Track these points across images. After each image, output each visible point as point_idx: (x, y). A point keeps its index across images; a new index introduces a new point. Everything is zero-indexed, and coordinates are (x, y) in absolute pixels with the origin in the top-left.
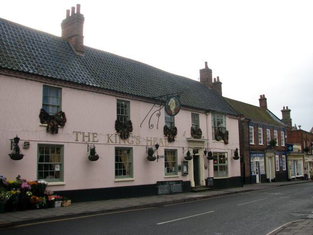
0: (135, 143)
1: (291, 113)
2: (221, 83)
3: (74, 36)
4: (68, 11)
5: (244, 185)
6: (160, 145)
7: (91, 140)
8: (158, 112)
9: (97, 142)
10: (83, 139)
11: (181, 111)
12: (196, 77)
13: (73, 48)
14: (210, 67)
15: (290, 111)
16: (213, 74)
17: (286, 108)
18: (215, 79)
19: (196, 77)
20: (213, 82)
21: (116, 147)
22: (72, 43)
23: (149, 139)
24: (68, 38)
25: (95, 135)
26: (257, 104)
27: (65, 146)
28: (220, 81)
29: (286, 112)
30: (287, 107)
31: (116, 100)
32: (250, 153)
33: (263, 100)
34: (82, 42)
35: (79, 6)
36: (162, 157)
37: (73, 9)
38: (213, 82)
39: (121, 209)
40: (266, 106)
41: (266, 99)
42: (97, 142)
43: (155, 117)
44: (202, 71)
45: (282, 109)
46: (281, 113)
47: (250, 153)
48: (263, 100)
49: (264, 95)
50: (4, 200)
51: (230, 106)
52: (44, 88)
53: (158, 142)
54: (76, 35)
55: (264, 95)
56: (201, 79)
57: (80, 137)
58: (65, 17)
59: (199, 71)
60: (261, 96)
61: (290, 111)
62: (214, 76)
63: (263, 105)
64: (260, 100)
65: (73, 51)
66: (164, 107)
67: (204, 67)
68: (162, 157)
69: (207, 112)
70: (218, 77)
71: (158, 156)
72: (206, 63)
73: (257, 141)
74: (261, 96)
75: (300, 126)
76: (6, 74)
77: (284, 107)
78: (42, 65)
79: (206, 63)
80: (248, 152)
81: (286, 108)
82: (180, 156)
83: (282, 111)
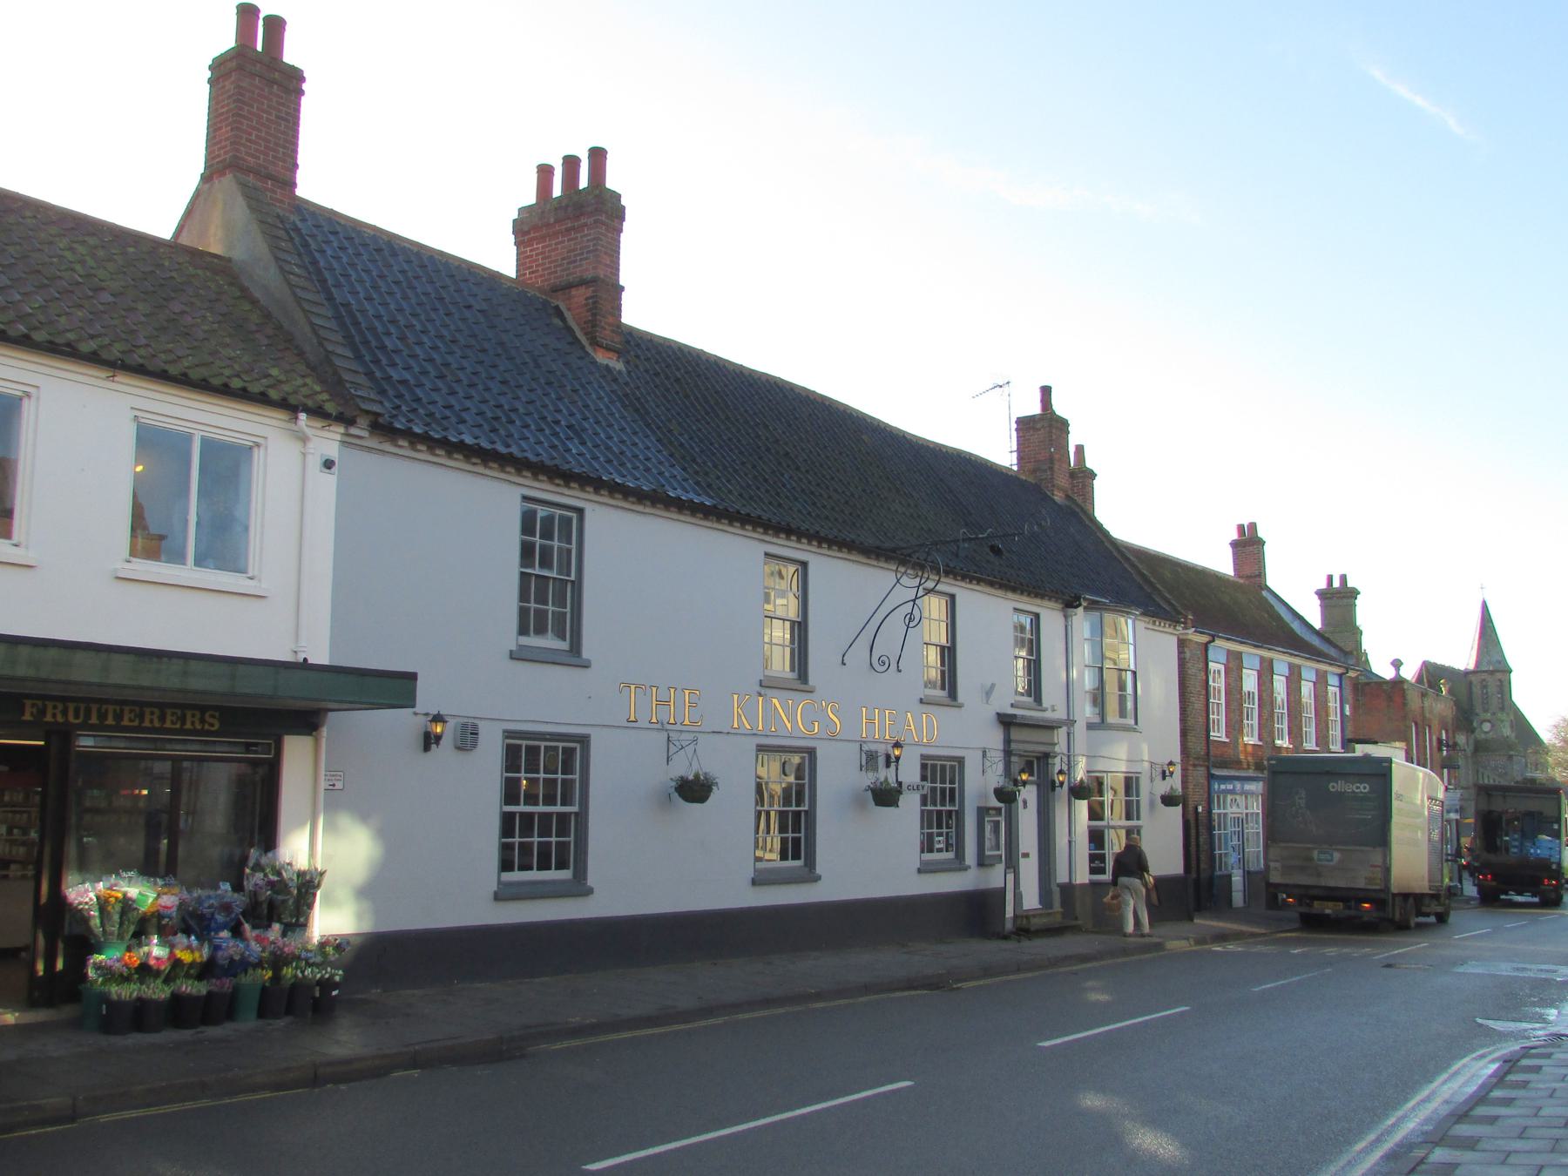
1: (1361, 604)
2: (1092, 475)
3: (583, 283)
4: (545, 172)
12: (1001, 451)
13: (579, 334)
14: (1060, 408)
15: (1354, 593)
17: (1336, 584)
21: (923, 757)
22: (573, 308)
24: (555, 290)
26: (1223, 563)
27: (593, 739)
28: (1089, 464)
29: (1339, 598)
30: (1343, 578)
31: (519, 499)
32: (1211, 777)
33: (1248, 545)
35: (598, 155)
36: (911, 788)
37: (571, 163)
40: (1260, 574)
41: (1261, 543)
44: (1025, 426)
45: (1323, 585)
46: (1316, 602)
47: (1211, 777)
48: (1248, 545)
49: (1253, 526)
50: (1536, 766)
54: (594, 281)
55: (1253, 526)
56: (1020, 459)
59: (1095, 471)
60: (1241, 528)
61: (1354, 593)
63: (1247, 571)
64: (1234, 544)
65: (583, 348)
67: (1035, 409)
71: (900, 784)
72: (1046, 392)
73: (1235, 727)
74: (1241, 528)
75: (1397, 664)
76: (1334, 717)
77: (1330, 578)
78: (508, 416)
79: (1046, 392)
80: (1202, 771)
81: (1336, 584)
82: (981, 781)
83: (1321, 594)
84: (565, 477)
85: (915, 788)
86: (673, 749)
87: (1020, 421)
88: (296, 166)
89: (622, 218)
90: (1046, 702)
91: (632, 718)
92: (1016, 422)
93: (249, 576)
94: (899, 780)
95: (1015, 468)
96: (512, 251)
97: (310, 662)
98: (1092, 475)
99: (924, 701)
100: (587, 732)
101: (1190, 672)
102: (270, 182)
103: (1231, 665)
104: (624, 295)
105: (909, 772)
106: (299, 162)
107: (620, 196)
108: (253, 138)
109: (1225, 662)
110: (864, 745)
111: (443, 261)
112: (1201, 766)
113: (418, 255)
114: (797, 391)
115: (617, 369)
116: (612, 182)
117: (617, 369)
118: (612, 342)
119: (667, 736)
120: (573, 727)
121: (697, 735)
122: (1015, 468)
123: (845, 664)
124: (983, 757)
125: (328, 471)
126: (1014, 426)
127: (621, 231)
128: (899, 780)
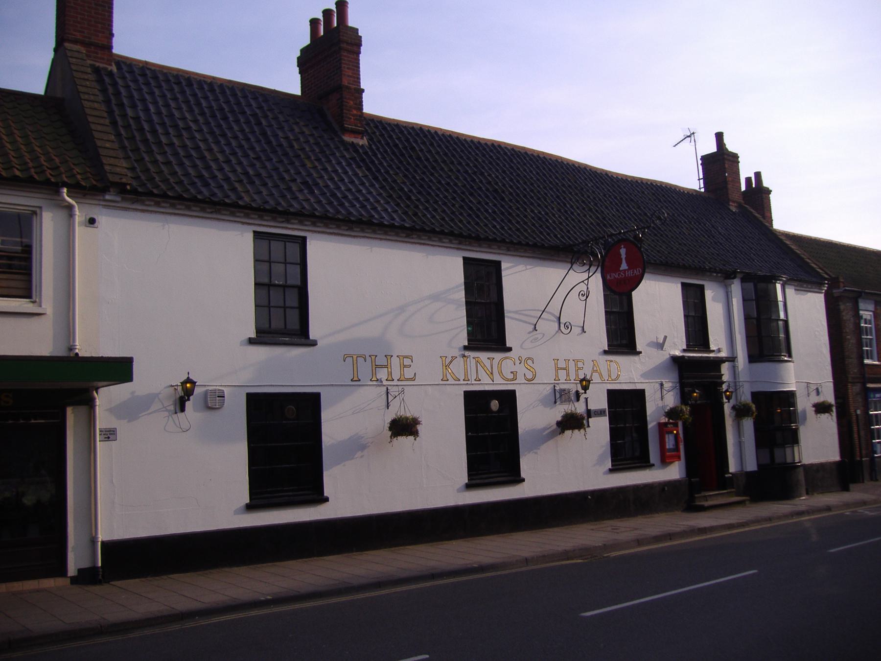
0: (521, 379)
2: (768, 192)
4: (314, 23)
5: (852, 486)
6: (596, 378)
7: (396, 376)
8: (583, 287)
9: (413, 379)
10: (557, 376)
11: (646, 275)
12: (722, 373)
14: (731, 145)
16: (741, 166)
18: (748, 180)
19: (722, 373)
20: (743, 188)
23: (562, 364)
25: (407, 362)
34: (359, 105)
36: (600, 413)
37: (327, 13)
38: (743, 188)
39: (482, 569)
42: (413, 379)
43: (574, 303)
44: (708, 161)
51: (625, 527)
52: (254, 235)
53: (586, 372)
57: (365, 369)
58: (306, 41)
62: (746, 171)
66: (599, 269)
67: (712, 148)
68: (600, 413)
69: (725, 276)
70: (758, 175)
72: (719, 136)
79: (719, 136)
84: (286, 215)
85: (599, 413)
86: (390, 398)
87: (703, 158)
88: (112, 35)
89: (359, 45)
90: (713, 347)
91: (355, 379)
92: (701, 159)
93: (32, 300)
94: (589, 408)
95: (703, 190)
96: (298, 78)
97: (80, 355)
98: (768, 192)
99: (252, 341)
100: (513, 389)
101: (844, 318)
102: (93, 47)
103: (878, 311)
104: (772, 197)
105: (598, 399)
106: (114, 32)
107: (357, 30)
108: (79, 19)
109: (873, 310)
110: (556, 385)
111: (230, 87)
112: (858, 382)
113: (450, 136)
114: (517, 150)
115: (360, 144)
116: (352, 22)
117: (360, 144)
118: (355, 126)
119: (386, 390)
120: (286, 388)
121: (744, 383)
122: (703, 190)
123: (585, 332)
124: (661, 388)
125: (92, 226)
126: (700, 162)
127: (359, 53)
128: (589, 408)
